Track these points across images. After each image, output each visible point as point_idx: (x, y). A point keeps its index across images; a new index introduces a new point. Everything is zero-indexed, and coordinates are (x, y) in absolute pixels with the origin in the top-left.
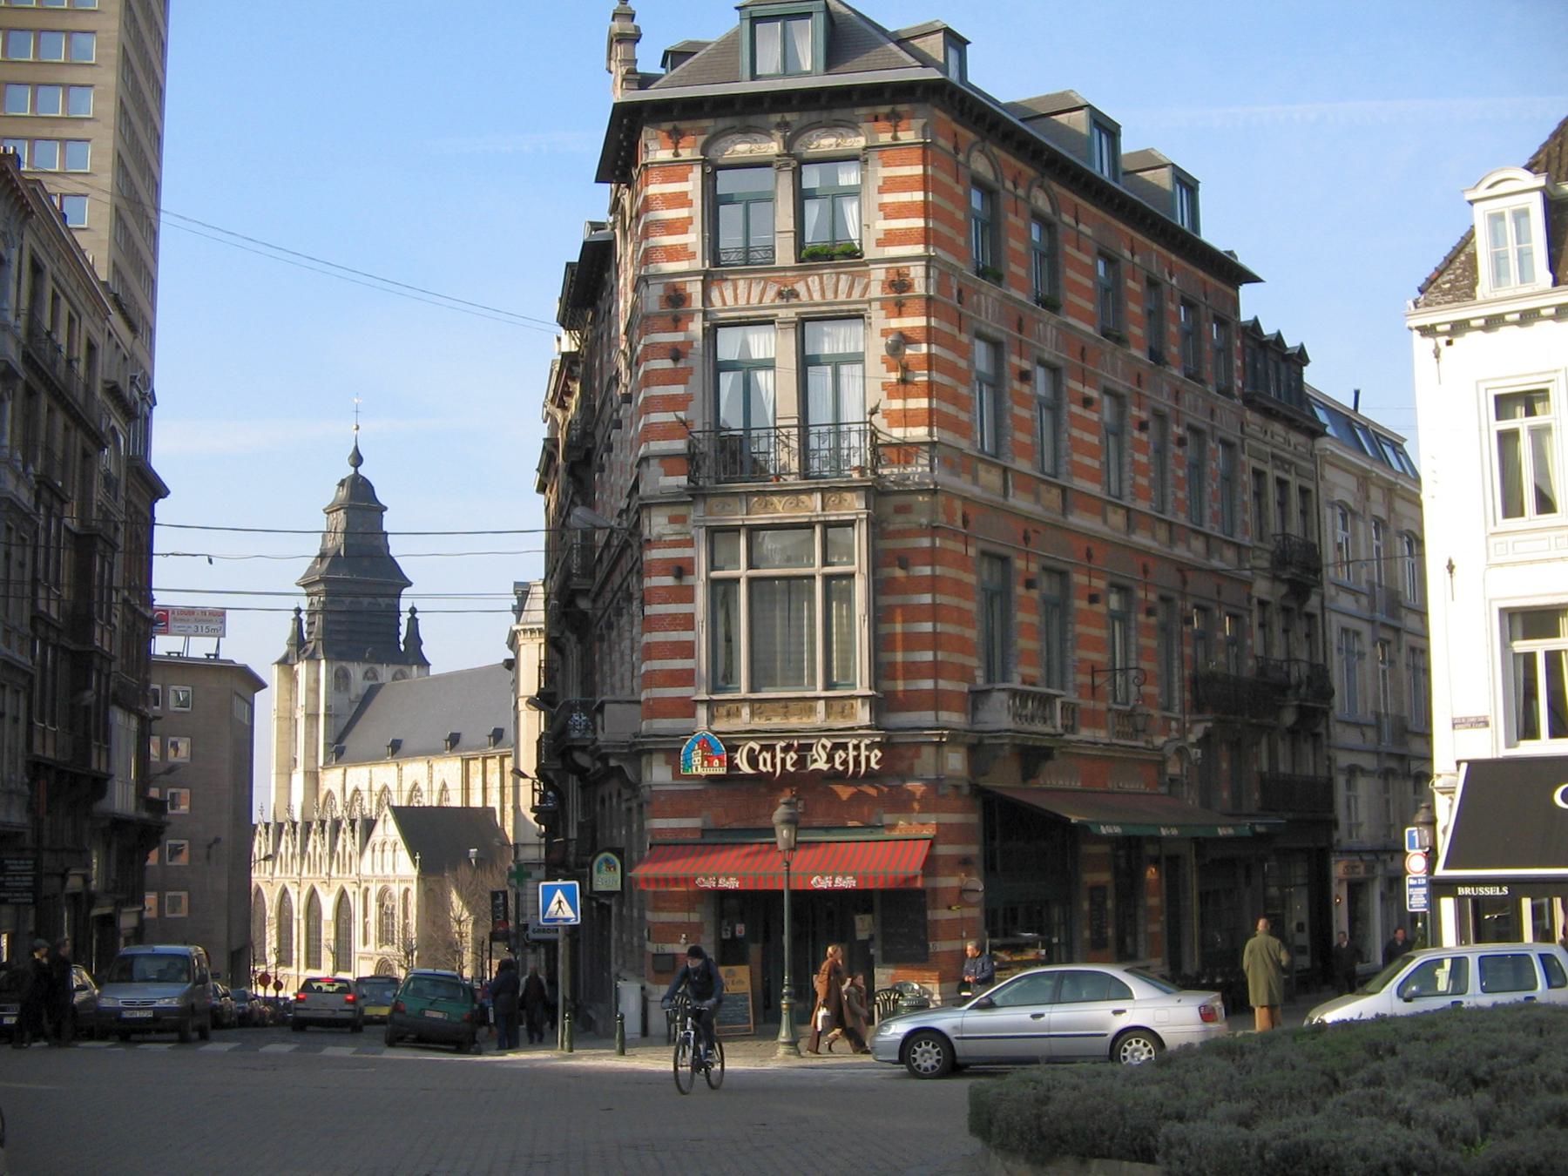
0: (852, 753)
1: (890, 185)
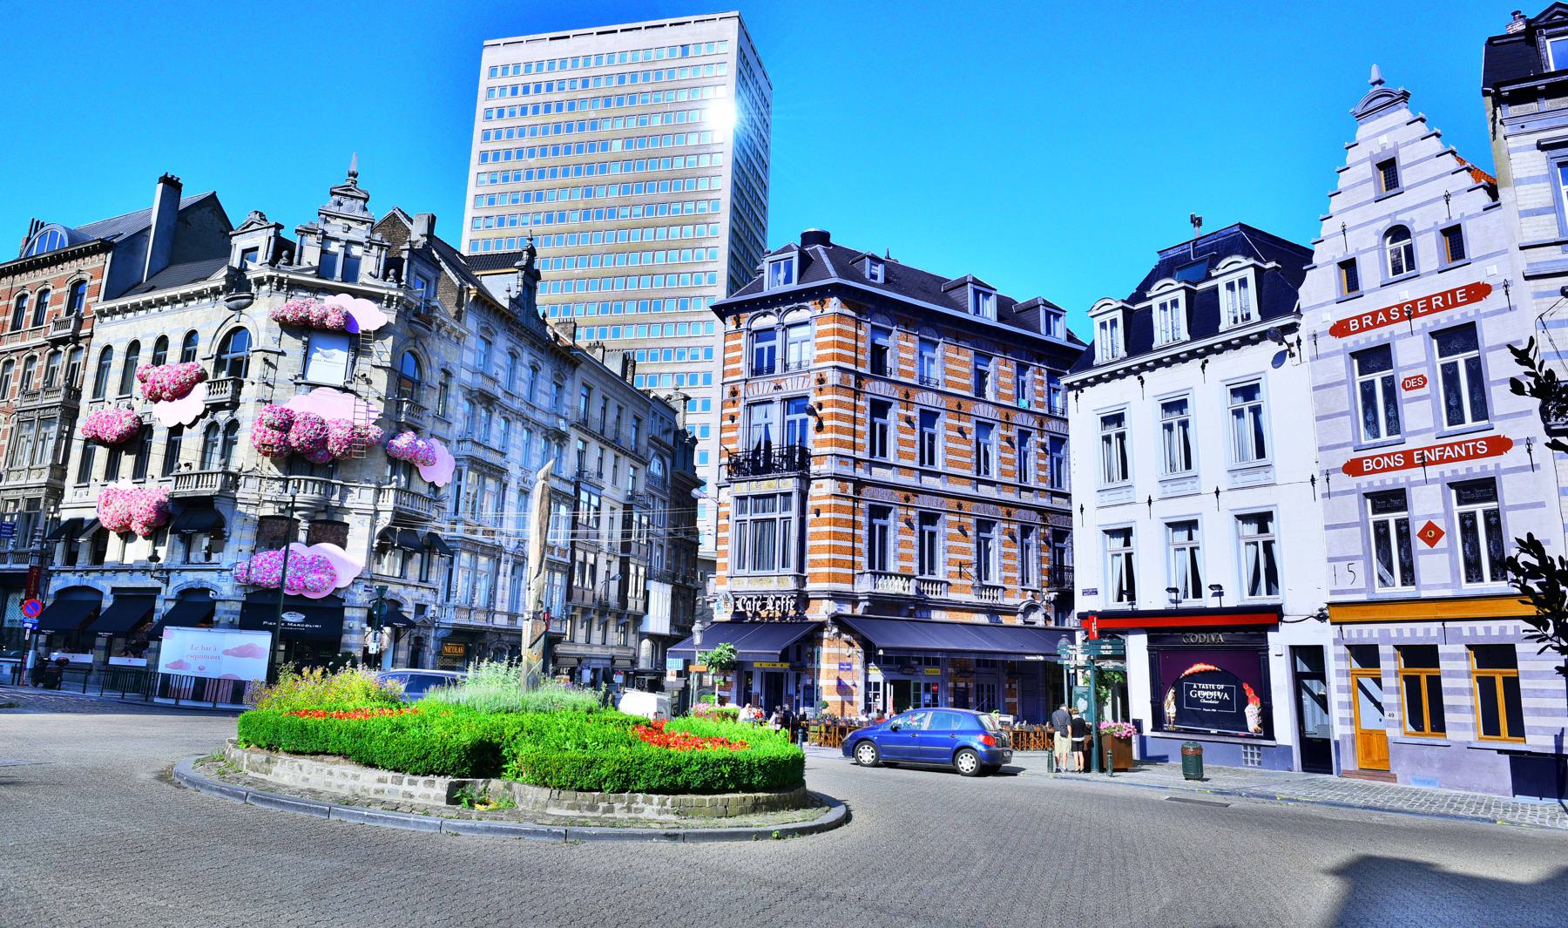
1: (820, 334)
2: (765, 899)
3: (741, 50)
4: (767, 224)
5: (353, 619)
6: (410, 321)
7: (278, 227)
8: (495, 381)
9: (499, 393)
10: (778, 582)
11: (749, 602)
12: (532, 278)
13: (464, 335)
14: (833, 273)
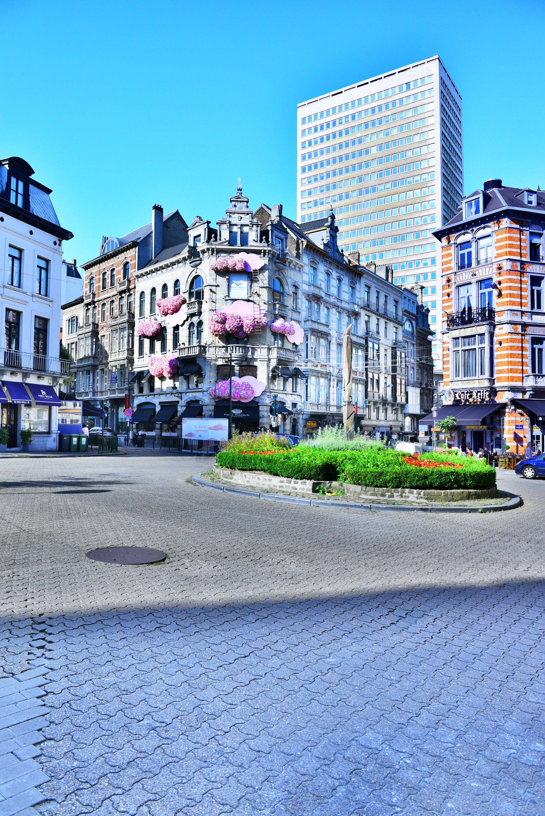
0: (482, 393)
2: (475, 540)
3: (442, 79)
4: (463, 181)
5: (264, 411)
6: (276, 262)
7: (208, 222)
8: (320, 288)
9: (323, 294)
10: (479, 382)
11: (463, 394)
12: (334, 230)
13: (302, 266)
14: (504, 203)
